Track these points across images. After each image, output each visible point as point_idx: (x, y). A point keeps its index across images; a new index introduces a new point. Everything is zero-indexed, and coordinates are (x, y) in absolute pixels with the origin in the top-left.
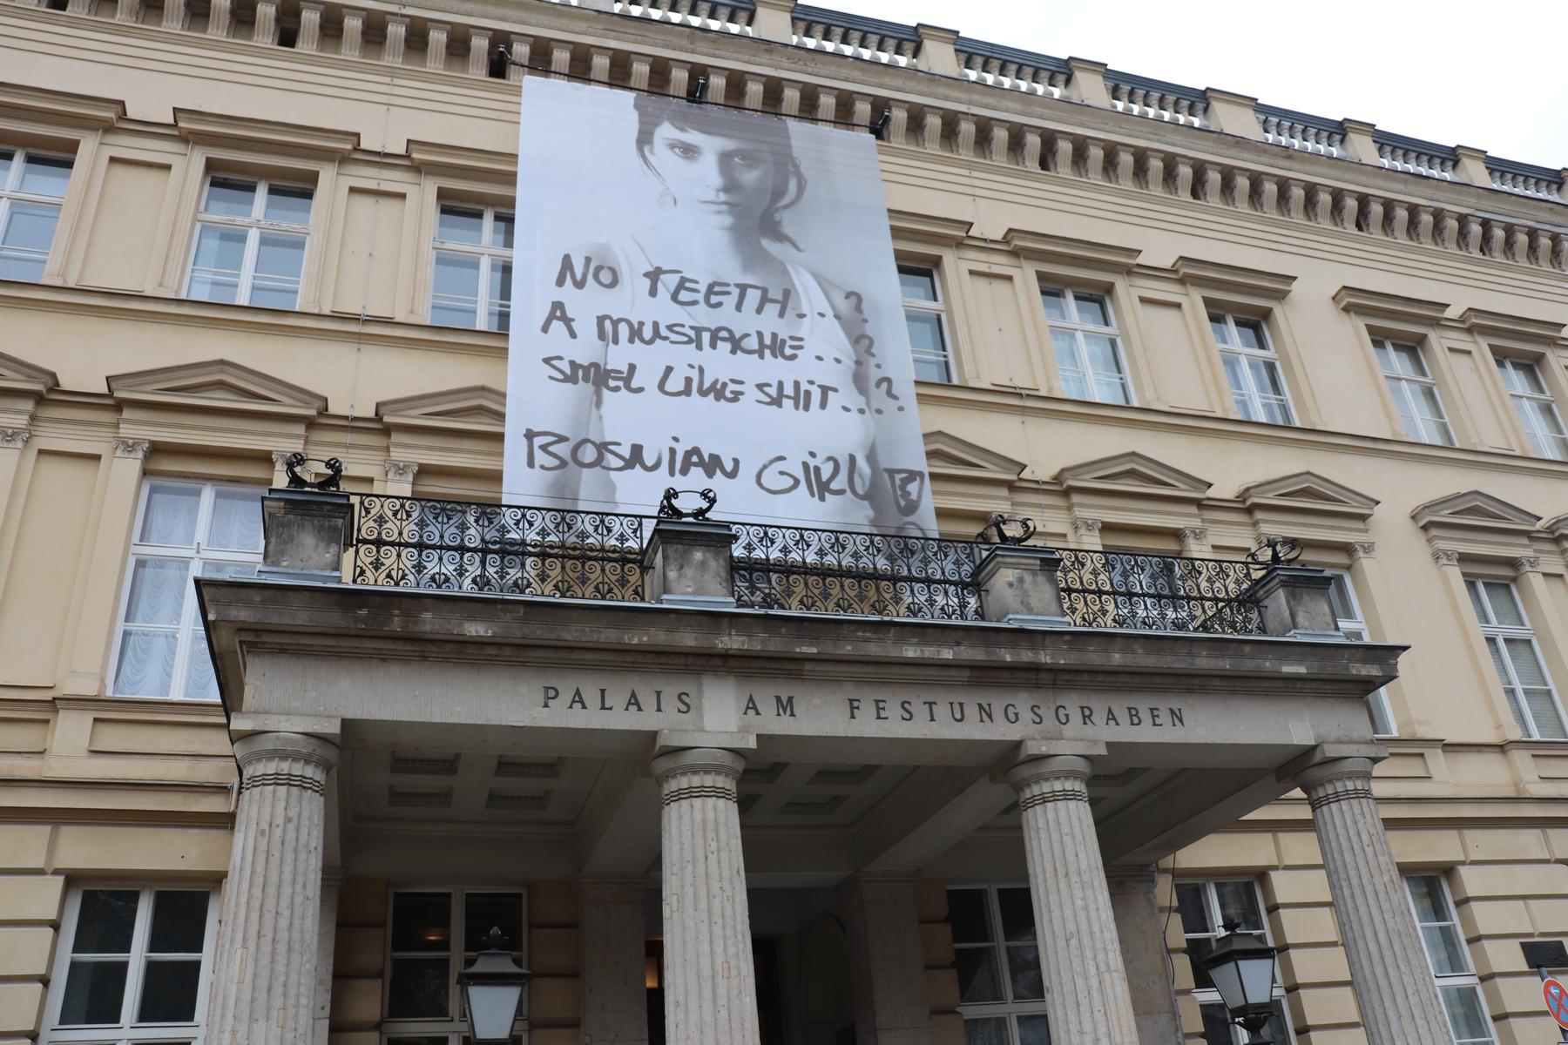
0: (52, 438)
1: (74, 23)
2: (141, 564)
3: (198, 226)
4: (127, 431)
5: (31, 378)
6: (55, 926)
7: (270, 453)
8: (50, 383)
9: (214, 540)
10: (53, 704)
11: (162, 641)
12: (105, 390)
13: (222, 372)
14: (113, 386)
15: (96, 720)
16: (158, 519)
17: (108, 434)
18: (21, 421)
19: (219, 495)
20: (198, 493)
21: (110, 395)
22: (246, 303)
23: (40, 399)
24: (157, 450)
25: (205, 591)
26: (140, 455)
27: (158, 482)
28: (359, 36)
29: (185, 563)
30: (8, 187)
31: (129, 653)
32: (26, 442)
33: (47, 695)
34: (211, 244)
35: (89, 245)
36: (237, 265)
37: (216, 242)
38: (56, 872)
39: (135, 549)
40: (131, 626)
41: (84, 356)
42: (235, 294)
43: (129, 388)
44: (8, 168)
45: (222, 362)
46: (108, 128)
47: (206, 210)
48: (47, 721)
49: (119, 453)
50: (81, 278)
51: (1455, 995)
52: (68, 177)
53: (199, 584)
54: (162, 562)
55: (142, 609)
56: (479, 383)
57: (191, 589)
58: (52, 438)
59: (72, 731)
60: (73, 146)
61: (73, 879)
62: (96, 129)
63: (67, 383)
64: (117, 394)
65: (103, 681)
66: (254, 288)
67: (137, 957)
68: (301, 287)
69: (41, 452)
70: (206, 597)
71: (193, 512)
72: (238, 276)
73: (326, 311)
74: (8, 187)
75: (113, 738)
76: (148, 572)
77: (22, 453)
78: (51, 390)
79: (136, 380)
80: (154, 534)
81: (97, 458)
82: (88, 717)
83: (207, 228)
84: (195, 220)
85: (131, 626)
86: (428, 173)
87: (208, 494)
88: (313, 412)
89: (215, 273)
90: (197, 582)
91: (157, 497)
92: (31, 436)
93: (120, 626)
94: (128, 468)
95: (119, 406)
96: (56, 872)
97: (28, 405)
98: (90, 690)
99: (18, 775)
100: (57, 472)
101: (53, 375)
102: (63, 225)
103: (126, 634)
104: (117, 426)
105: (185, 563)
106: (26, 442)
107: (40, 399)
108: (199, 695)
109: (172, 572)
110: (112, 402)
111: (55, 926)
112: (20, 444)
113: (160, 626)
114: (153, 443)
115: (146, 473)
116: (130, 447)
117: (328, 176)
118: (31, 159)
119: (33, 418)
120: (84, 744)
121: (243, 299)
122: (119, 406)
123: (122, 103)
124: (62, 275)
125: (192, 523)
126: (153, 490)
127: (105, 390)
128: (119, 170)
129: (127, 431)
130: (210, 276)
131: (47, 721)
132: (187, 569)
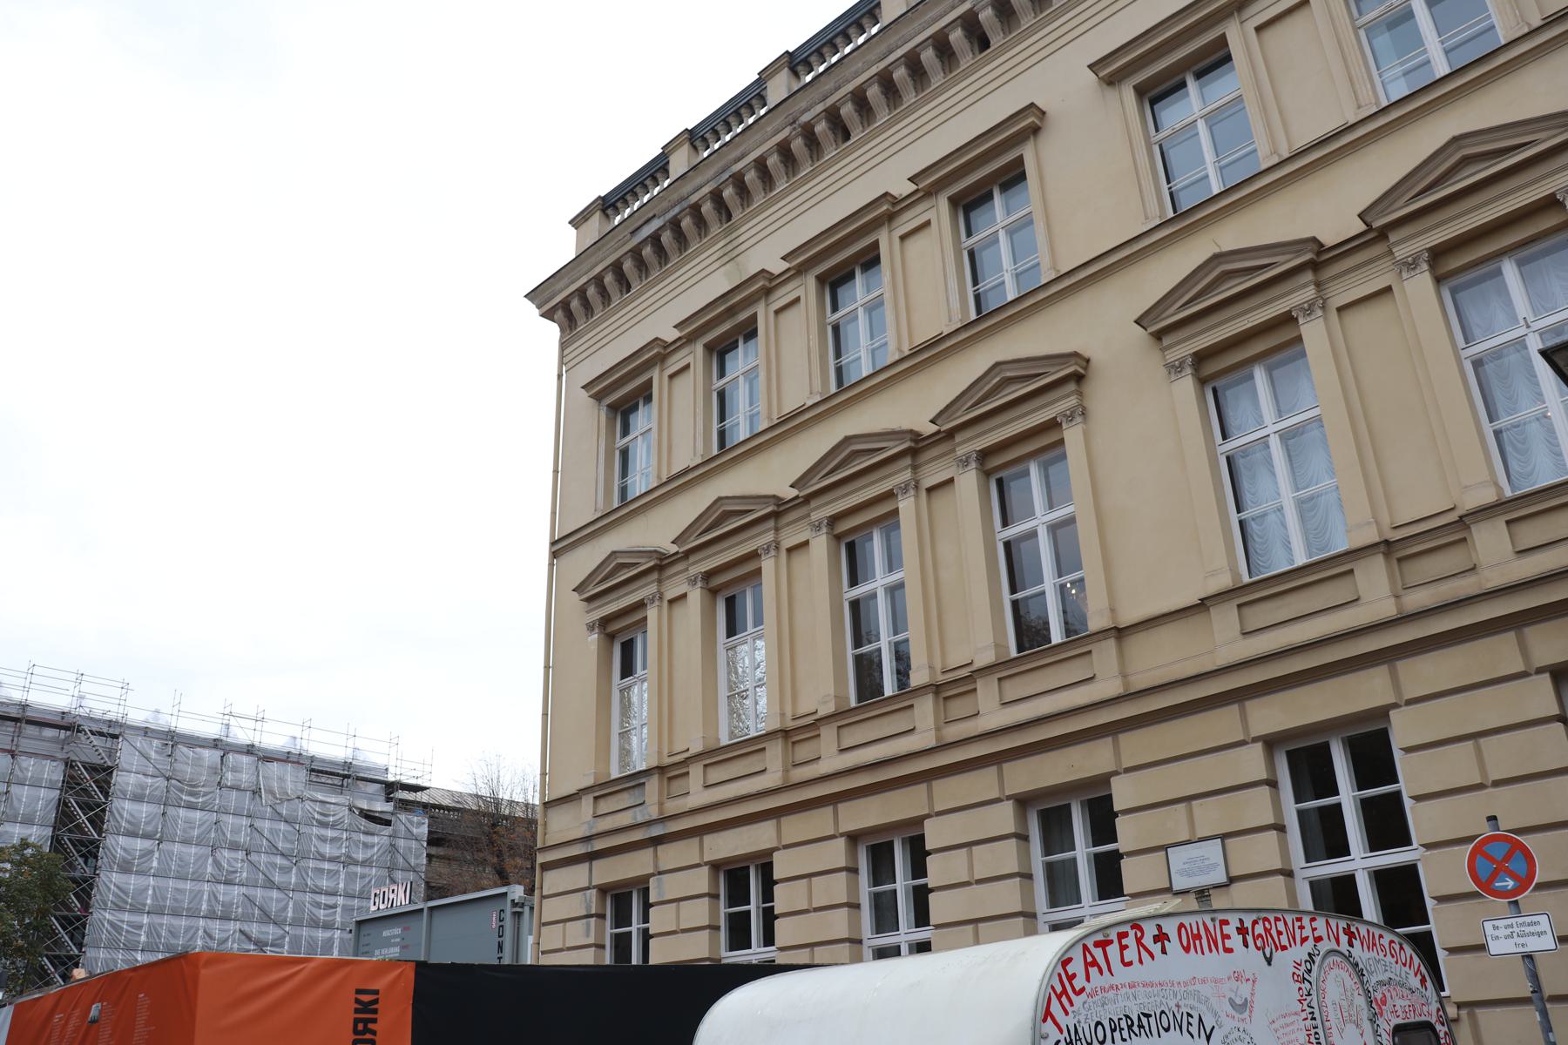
0: (1344, 293)
1: (863, 142)
2: (1478, 364)
3: (1362, 33)
4: (1401, 252)
5: (1298, 253)
6: (1272, 783)
7: (1553, 195)
8: (1316, 248)
9: (1539, 308)
10: (971, 678)
11: (1535, 426)
12: (1363, 227)
13: (1460, 148)
14: (1368, 219)
15: (1508, 522)
16: (1473, 317)
17: (1386, 263)
18: (1310, 293)
19: (1520, 264)
20: (1499, 272)
21: (1370, 229)
22: (1447, 71)
23: (1314, 266)
24: (1437, 255)
25: (1556, 358)
26: (1425, 266)
27: (1455, 282)
28: (965, 41)
29: (1520, 343)
30: (1196, 109)
31: (1509, 449)
32: (1323, 307)
33: (1453, 517)
34: (1383, 40)
35: (1281, 113)
36: (1418, 41)
37: (1387, 35)
38: (1255, 740)
39: (1464, 354)
40: (1498, 424)
41: (1330, 209)
42: (1432, 72)
43: (1383, 213)
44: (1187, 94)
45: (1455, 139)
46: (890, 217)
47: (1360, 14)
48: (1464, 540)
49: (1405, 275)
50: (911, 342)
51: (1315, 818)
52: (1233, 68)
53: (1546, 354)
54: (1497, 353)
55: (1247, 497)
56: (1209, 255)
57: (1543, 368)
58: (1344, 293)
59: (987, 692)
60: (1222, 41)
61: (1271, 743)
62: (1027, 138)
63: (1329, 239)
64: (1376, 224)
65: (1496, 484)
66: (1447, 52)
67: (1348, 796)
68: (1495, 20)
69: (1340, 310)
70: (1561, 364)
71: (1504, 291)
72: (1425, 51)
73: (1537, 23)
74: (1196, 109)
75: (1532, 533)
76: (1489, 368)
77: (1326, 319)
78: (1319, 253)
79: (1386, 203)
80: (1476, 331)
81: (1389, 289)
82: (1500, 523)
83: (1370, 29)
84: (1356, 29)
85: (1498, 424)
86: (1120, 81)
87: (1259, 374)
88: (1308, 257)
89: (1402, 64)
90: (1543, 353)
91: (1461, 296)
92: (1325, 301)
93: (1488, 430)
94: (1421, 284)
95: (1383, 234)
96: (1255, 740)
97: (1309, 276)
98: (1489, 497)
99: (1462, 594)
100: (1361, 321)
101: (1314, 240)
102: (1252, 109)
103: (1497, 433)
104: (1391, 253)
105: (1520, 343)
106: (1323, 307)
107: (1314, 266)
108: (1322, 550)
109: (1513, 358)
110: (1376, 233)
111: (1272, 783)
112: (1320, 313)
113: (1527, 411)
114: (1430, 250)
115: (1438, 280)
116: (1411, 265)
117: (763, 312)
118: (1199, 75)
119: (1318, 285)
120: (834, 748)
121: (1442, 68)
122: (1383, 234)
123: (886, 194)
124: (1275, 152)
125: (1509, 303)
126: (1454, 292)
127: (1363, 227)
128: (1269, 34)
129: (1401, 252)
130: (1400, 69)
131: (1464, 540)
132: (1526, 348)
